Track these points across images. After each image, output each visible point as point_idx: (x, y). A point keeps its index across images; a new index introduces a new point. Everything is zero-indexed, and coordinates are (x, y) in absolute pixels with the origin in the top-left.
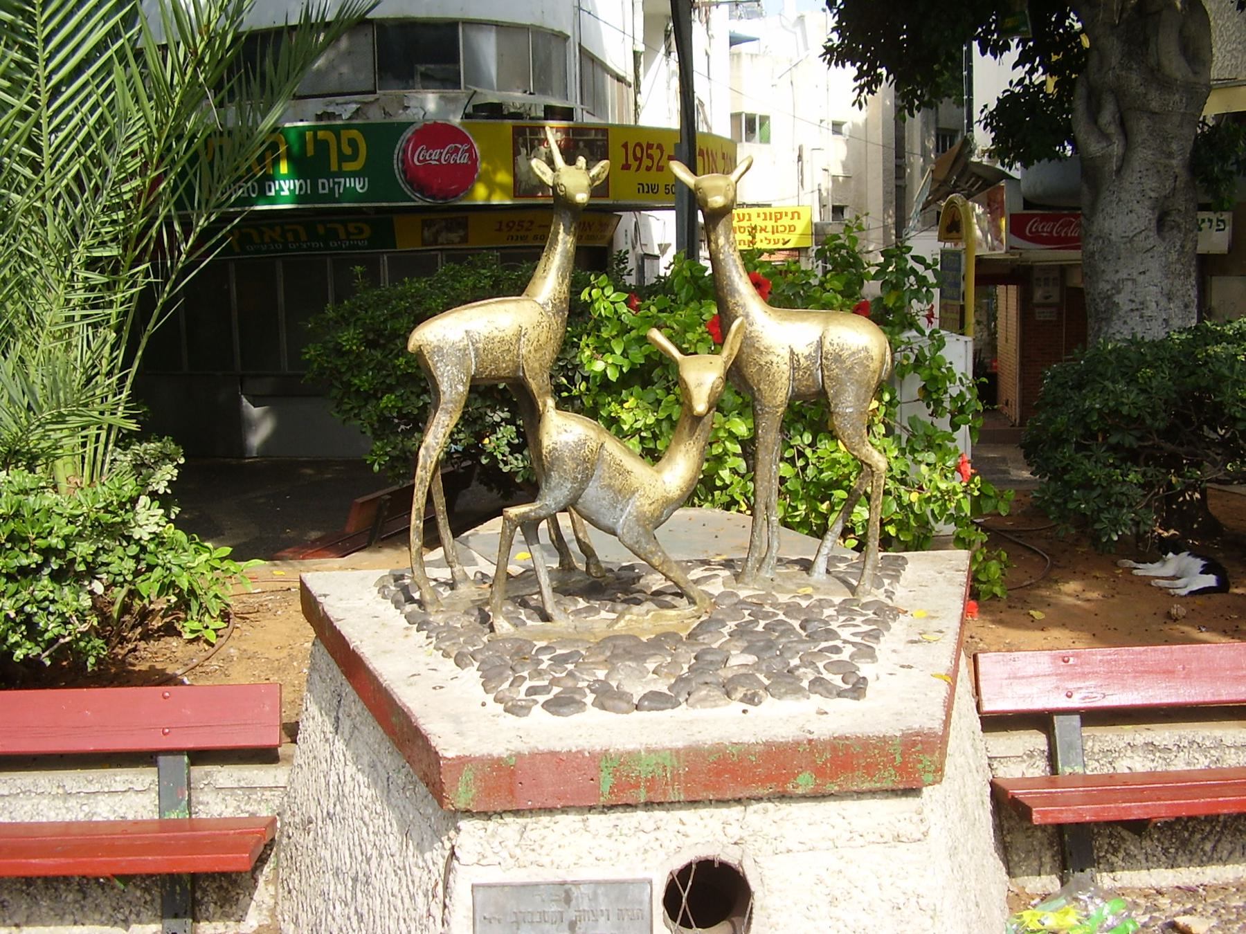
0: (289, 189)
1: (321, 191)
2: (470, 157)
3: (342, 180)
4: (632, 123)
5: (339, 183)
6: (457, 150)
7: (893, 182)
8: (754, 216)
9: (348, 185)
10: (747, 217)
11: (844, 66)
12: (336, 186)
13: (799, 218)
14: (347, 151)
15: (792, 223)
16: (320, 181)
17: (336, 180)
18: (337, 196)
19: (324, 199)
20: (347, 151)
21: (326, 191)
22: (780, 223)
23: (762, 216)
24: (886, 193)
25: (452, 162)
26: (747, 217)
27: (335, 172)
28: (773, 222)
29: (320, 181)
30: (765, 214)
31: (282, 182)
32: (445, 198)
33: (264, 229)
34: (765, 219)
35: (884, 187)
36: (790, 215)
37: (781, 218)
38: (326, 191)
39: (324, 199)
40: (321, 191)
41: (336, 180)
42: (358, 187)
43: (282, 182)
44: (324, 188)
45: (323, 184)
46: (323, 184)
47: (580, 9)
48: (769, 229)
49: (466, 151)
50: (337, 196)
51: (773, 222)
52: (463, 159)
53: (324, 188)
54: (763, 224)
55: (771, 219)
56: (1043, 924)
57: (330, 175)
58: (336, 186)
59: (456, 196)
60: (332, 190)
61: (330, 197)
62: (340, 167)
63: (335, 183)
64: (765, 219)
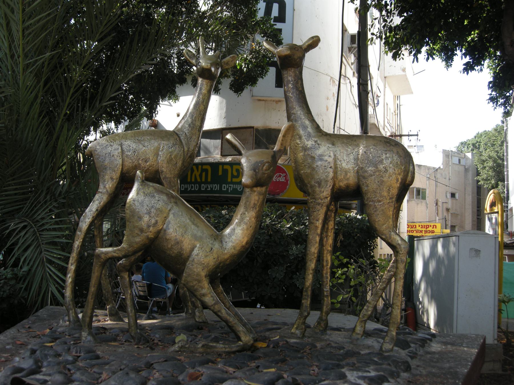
0: (210, 188)
1: (223, 189)
2: (286, 179)
3: (232, 185)
4: (332, 133)
5: (231, 187)
6: (280, 176)
7: (476, 217)
8: (417, 226)
9: (234, 187)
10: (414, 226)
11: (433, 59)
12: (230, 188)
13: (436, 228)
14: (235, 174)
15: (433, 229)
16: (223, 185)
17: (230, 185)
18: (229, 191)
19: (224, 192)
20: (235, 174)
21: (225, 189)
22: (428, 229)
23: (421, 226)
24: (473, 221)
25: (278, 181)
26: (414, 226)
27: (229, 182)
28: (425, 229)
29: (223, 185)
30: (421, 225)
31: (208, 185)
32: (274, 195)
33: (203, 206)
34: (422, 228)
35: (472, 219)
36: (432, 226)
37: (428, 228)
38: (225, 189)
39: (224, 192)
40: (223, 189)
41: (230, 185)
42: (238, 188)
43: (208, 185)
44: (224, 188)
45: (224, 187)
46: (224, 187)
47: (340, 128)
48: (423, 232)
49: (284, 176)
50: (229, 191)
51: (425, 229)
52: (282, 179)
53: (224, 188)
54: (421, 229)
55: (424, 228)
56: (377, 18)
57: (227, 183)
58: (230, 188)
59: (278, 194)
60: (228, 189)
61: (227, 192)
62: (232, 179)
63: (229, 186)
64: (422, 228)
